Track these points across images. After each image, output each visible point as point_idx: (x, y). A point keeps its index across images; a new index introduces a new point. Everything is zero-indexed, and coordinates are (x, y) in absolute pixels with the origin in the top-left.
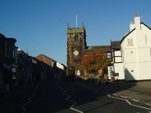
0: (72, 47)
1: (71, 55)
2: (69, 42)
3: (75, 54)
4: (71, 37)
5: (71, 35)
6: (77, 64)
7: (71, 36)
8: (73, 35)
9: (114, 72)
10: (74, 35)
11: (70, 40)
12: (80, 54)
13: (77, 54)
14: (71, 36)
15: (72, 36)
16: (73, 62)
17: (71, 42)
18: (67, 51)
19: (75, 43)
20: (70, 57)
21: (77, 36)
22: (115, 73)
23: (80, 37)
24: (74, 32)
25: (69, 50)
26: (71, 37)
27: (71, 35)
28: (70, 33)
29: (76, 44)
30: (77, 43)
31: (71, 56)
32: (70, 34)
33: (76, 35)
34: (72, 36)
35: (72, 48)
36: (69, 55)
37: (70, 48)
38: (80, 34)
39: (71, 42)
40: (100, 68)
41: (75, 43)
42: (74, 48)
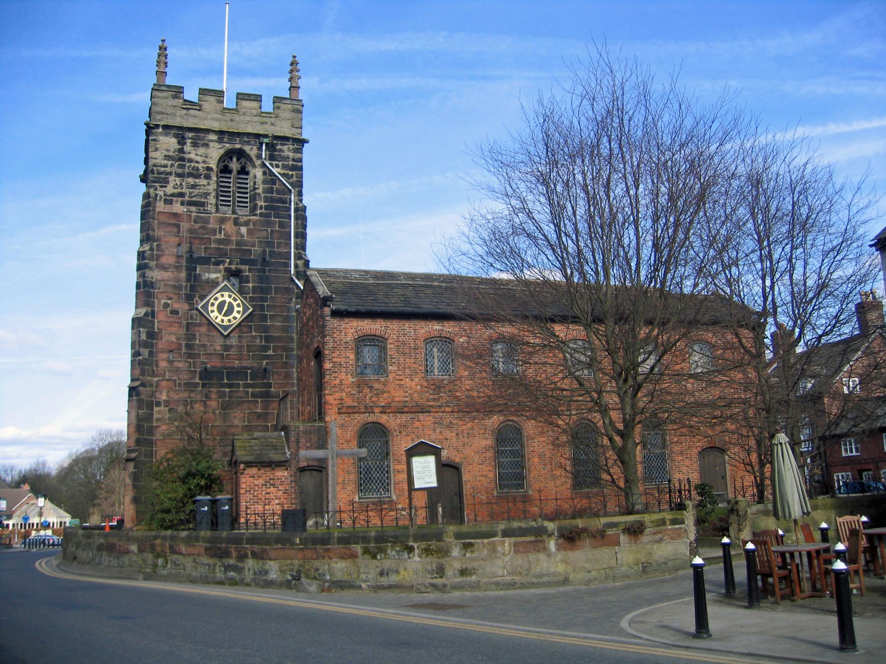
0: (185, 247)
1: (171, 324)
2: (160, 206)
3: (216, 317)
4: (180, 157)
5: (182, 141)
6: (226, 407)
7: (181, 151)
8: (201, 150)
9: (639, 366)
10: (215, 152)
11: (170, 190)
12: (264, 318)
13: (237, 315)
14: (181, 151)
15: (192, 153)
16: (190, 386)
17: (177, 208)
18: (303, 197)
19: (222, 220)
20: (161, 344)
21: (234, 165)
22: (434, 484)
23: (267, 172)
24: (216, 126)
25: (155, 275)
26: (180, 157)
27: (188, 147)
28: (177, 122)
29: (229, 227)
30: (236, 222)
31: (170, 336)
32: (180, 132)
33: (228, 155)
34: (192, 153)
35: (193, 262)
36: (161, 316)
37: (164, 260)
38: (271, 147)
39: (177, 208)
40: (738, 243)
41: (222, 220)
42: (205, 261)
